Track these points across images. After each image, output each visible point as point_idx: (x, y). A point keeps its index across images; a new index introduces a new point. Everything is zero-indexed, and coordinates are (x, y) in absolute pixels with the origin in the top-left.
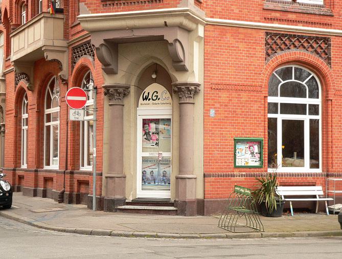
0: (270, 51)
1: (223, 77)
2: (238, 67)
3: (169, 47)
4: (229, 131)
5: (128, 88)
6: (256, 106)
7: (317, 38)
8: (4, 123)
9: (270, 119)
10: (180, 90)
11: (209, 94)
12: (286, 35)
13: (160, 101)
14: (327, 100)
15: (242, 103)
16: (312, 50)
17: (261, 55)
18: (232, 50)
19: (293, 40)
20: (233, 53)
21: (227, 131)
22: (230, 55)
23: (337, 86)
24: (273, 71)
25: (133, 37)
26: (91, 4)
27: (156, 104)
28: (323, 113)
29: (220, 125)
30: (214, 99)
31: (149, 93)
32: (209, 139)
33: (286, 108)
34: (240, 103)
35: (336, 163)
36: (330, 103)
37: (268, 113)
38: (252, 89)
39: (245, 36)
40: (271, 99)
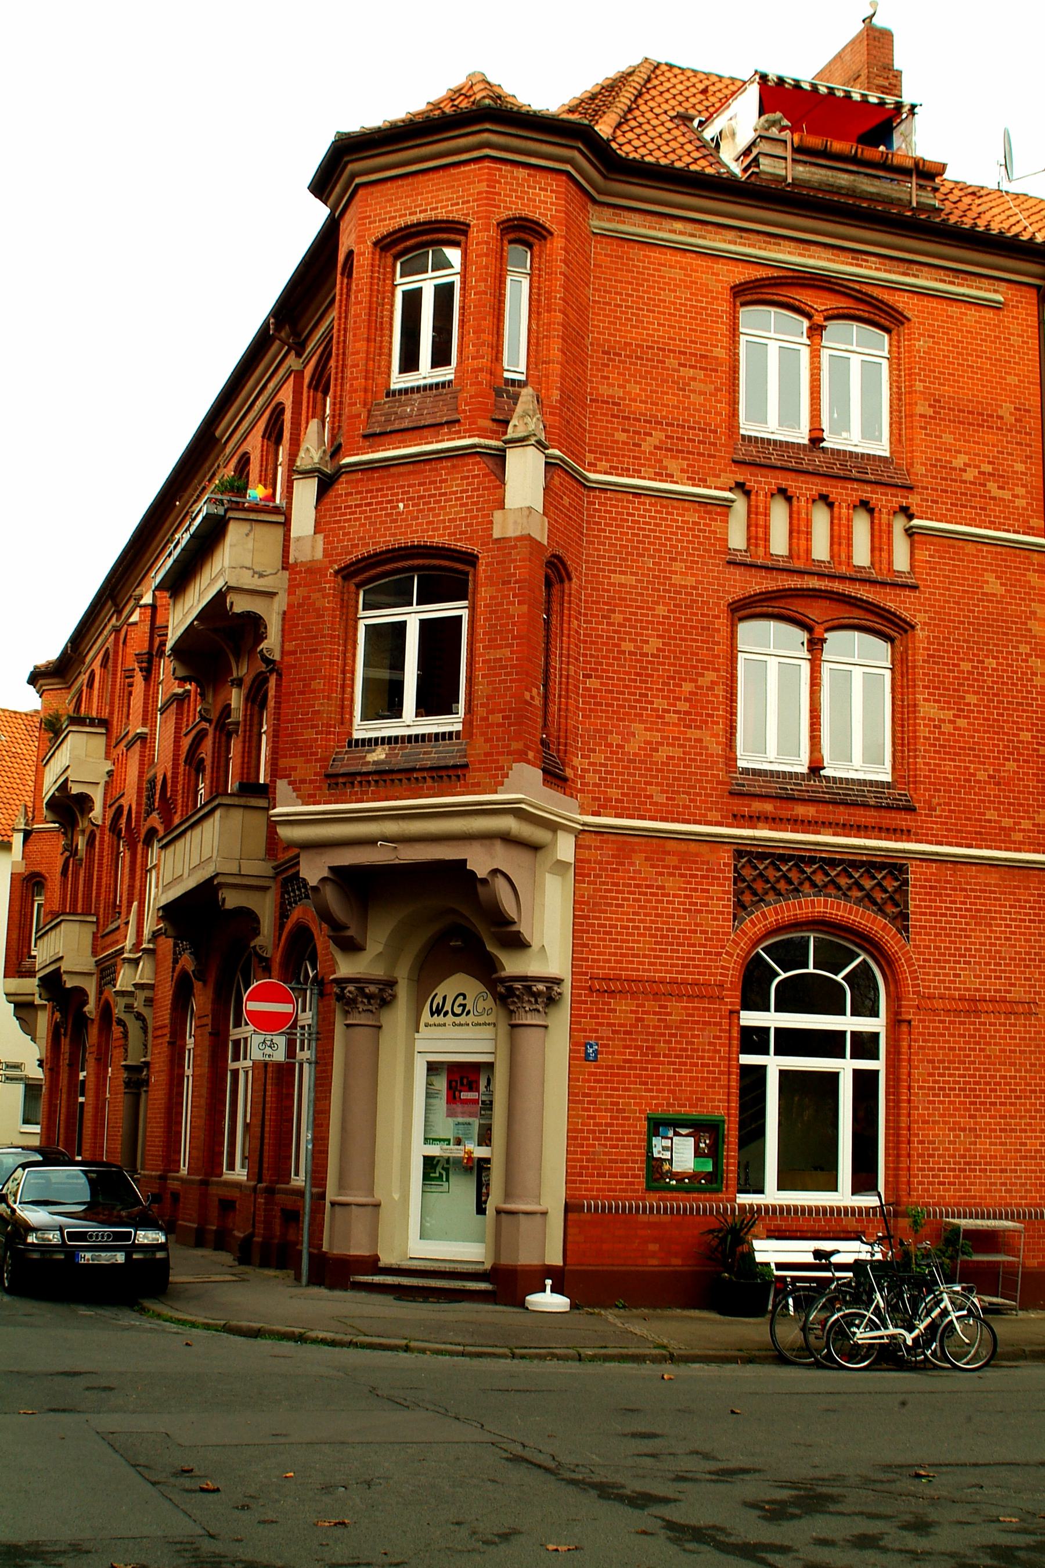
0: (747, 898)
1: (621, 962)
2: (662, 937)
3: (480, 889)
4: (634, 1097)
5: (391, 984)
6: (704, 1037)
7: (872, 865)
8: (148, 1059)
9: (746, 1069)
10: (511, 991)
11: (586, 1002)
12: (791, 857)
13: (470, 1019)
14: (900, 1021)
15: (669, 1028)
16: (859, 894)
17: (724, 906)
18: (646, 894)
19: (809, 870)
20: (650, 901)
21: (629, 1097)
22: (640, 907)
23: (924, 987)
24: (755, 945)
25: (397, 862)
26: (303, 781)
27: (461, 1025)
28: (888, 1052)
29: (612, 1082)
30: (596, 1017)
31: (445, 998)
32: (582, 1116)
33: (792, 1042)
34: (666, 1028)
35: (920, 1183)
36: (904, 1028)
37: (743, 1052)
38: (702, 992)
39: (681, 861)
40: (750, 1018)
